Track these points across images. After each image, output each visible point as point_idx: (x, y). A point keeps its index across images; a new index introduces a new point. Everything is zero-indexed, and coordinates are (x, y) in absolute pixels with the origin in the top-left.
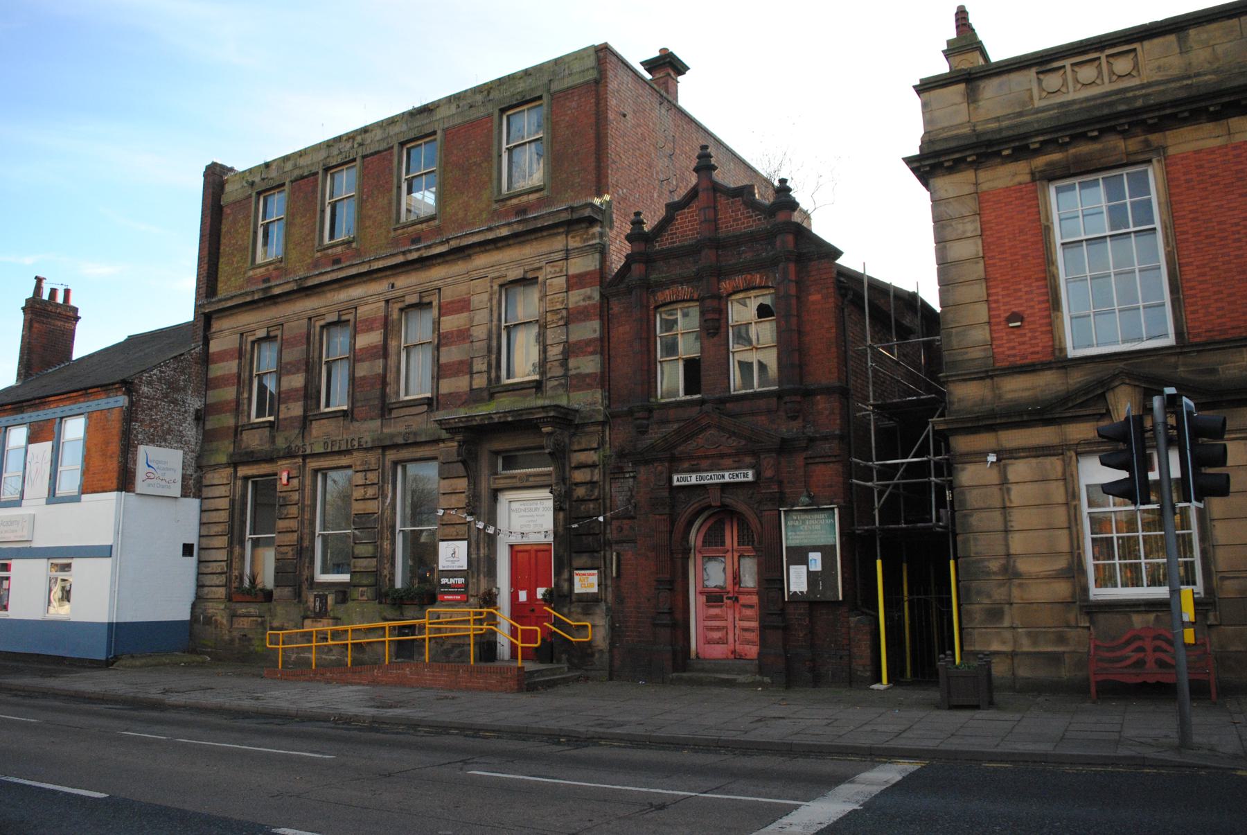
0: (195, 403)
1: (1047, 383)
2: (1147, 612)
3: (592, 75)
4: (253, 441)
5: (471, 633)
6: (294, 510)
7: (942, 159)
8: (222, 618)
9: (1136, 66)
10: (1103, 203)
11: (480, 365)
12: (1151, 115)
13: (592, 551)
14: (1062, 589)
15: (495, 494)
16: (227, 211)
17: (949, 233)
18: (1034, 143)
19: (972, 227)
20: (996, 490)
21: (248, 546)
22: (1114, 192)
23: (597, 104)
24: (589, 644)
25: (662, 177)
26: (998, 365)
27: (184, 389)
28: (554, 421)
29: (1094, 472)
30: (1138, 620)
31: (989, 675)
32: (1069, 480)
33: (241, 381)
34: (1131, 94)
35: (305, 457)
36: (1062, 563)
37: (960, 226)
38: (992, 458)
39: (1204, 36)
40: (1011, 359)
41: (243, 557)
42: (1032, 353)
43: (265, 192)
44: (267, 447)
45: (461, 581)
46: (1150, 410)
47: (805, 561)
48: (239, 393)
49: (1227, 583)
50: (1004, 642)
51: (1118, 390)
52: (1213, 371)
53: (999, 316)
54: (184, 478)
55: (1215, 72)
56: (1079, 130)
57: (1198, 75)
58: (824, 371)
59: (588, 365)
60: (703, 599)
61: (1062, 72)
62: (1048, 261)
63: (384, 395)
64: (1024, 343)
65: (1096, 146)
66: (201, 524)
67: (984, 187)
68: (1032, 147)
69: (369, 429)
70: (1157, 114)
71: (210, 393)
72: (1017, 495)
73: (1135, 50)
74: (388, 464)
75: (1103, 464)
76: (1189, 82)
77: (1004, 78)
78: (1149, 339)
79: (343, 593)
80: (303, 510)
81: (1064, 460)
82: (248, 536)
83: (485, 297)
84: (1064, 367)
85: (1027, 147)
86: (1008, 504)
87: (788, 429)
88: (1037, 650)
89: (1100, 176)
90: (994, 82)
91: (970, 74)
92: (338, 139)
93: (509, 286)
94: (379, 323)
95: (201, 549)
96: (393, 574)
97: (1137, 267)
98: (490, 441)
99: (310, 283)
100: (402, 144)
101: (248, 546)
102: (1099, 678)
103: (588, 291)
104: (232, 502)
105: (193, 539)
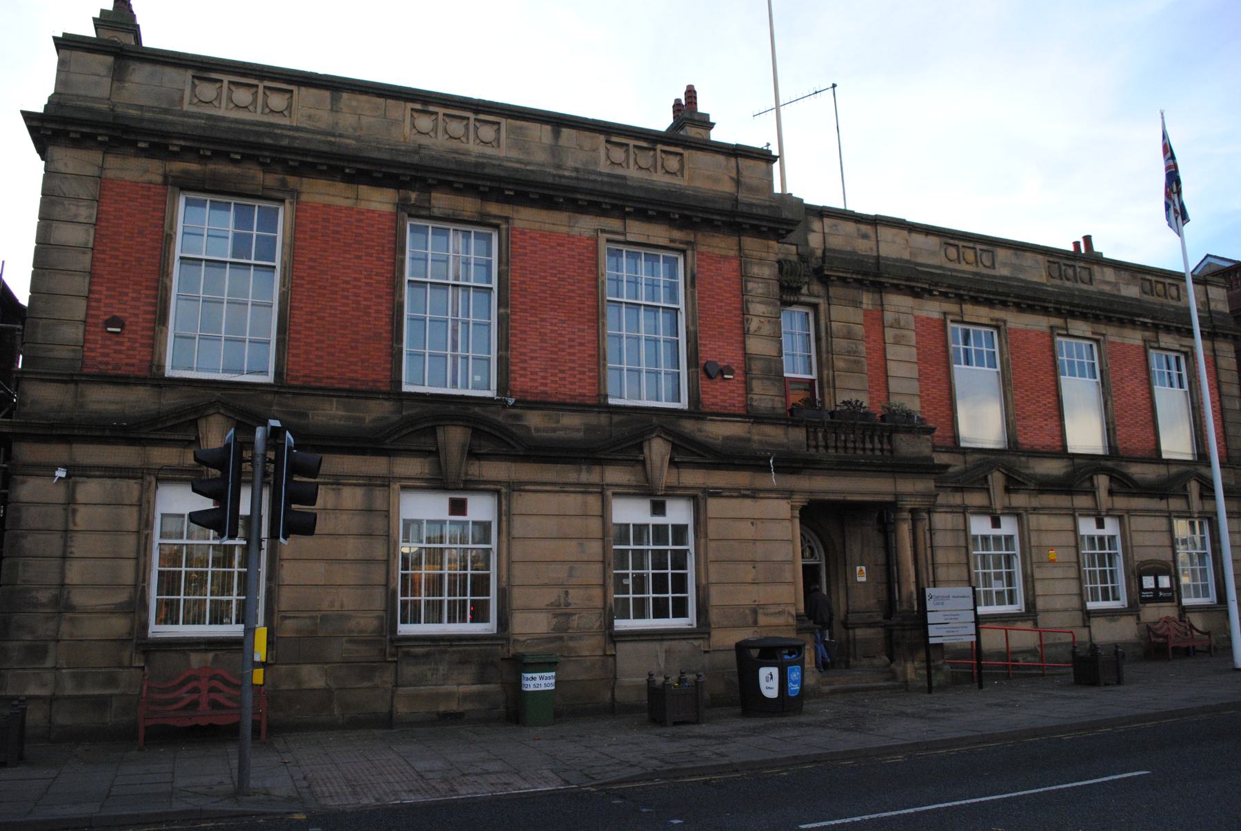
1: (138, 399)
2: (206, 651)
7: (70, 128)
9: (289, 107)
10: (231, 229)
12: (293, 157)
14: (119, 625)
17: (58, 212)
18: (175, 145)
19: (85, 213)
20: (59, 511)
22: (243, 220)
26: (86, 371)
29: (179, 501)
30: (196, 660)
31: (23, 722)
32: (144, 507)
34: (279, 131)
36: (123, 597)
37: (73, 208)
39: (354, 103)
40: (103, 367)
42: (127, 364)
46: (251, 444)
49: (287, 622)
50: (44, 685)
51: (211, 419)
52: (304, 415)
53: (97, 317)
55: (357, 139)
56: (224, 148)
57: (341, 136)
61: (218, 85)
62: (163, 271)
64: (120, 352)
65: (236, 170)
67: (110, 174)
68: (171, 148)
70: (299, 158)
72: (83, 517)
73: (291, 91)
75: (194, 490)
76: (333, 139)
77: (158, 68)
78: (249, 373)
81: (142, 485)
84: (159, 386)
85: (166, 146)
86: (71, 527)
88: (81, 693)
89: (233, 201)
90: (148, 68)
91: (121, 49)
97: (250, 300)
102: (150, 723)
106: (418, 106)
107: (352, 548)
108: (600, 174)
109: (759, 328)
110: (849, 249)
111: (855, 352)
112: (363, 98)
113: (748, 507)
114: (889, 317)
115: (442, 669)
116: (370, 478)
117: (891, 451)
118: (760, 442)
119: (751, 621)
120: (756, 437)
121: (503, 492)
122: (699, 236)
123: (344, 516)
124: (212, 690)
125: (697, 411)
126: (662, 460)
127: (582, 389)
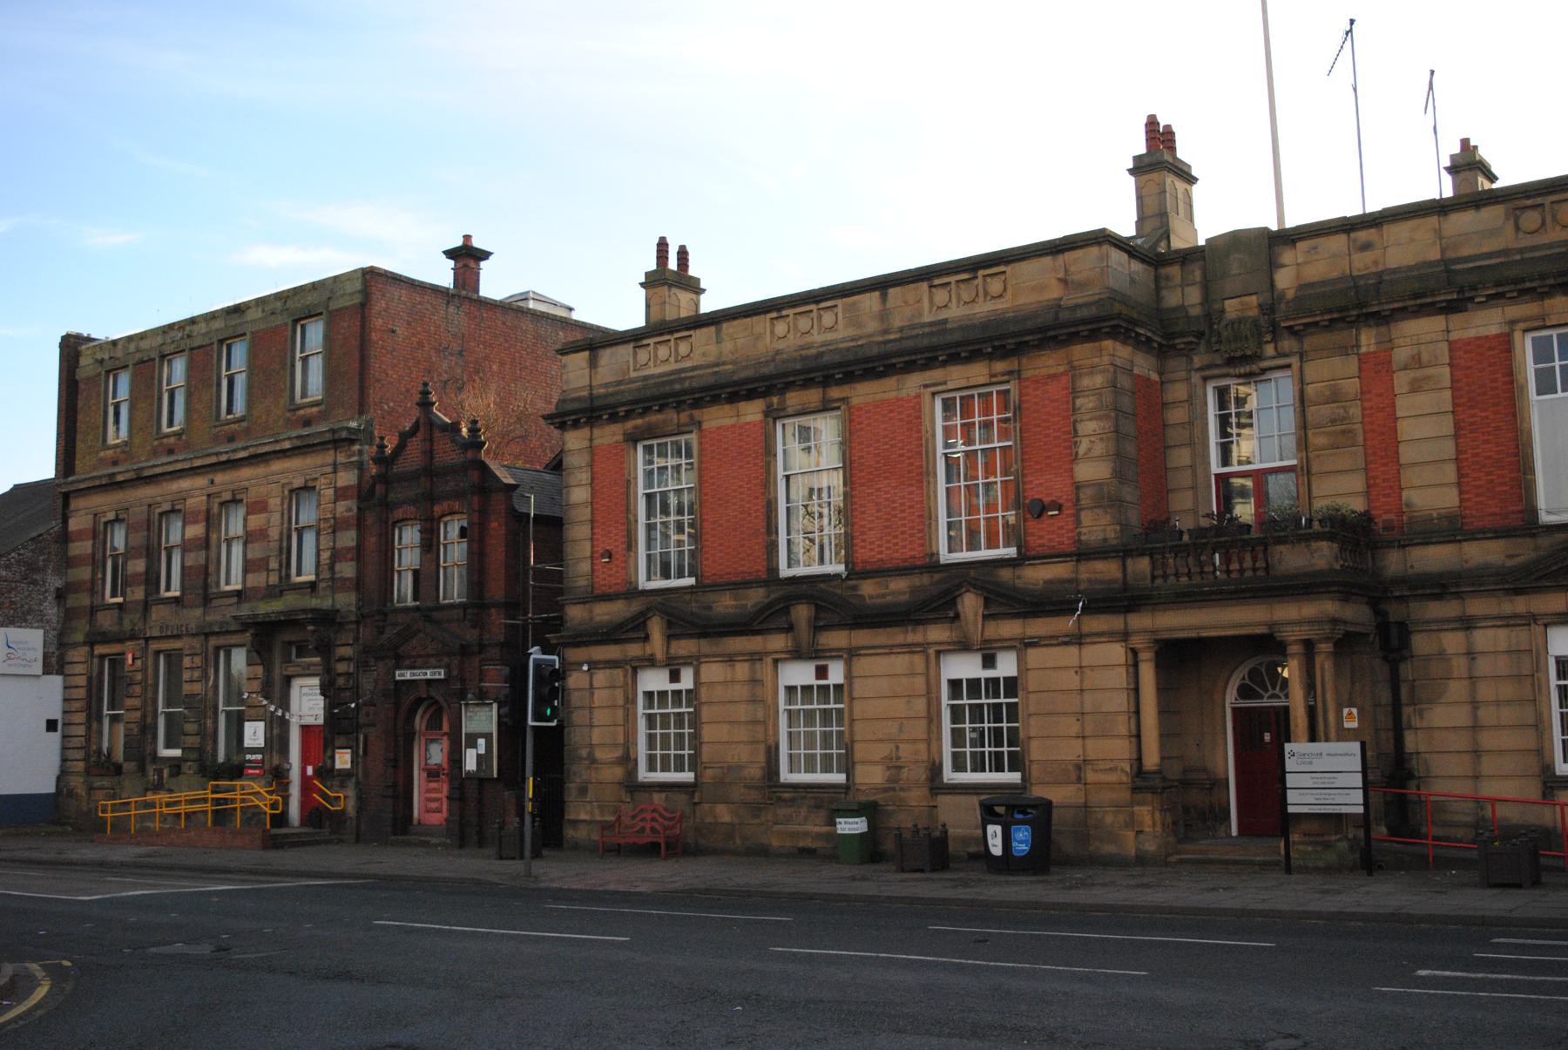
0: (55, 582)
3: (357, 299)
4: (106, 621)
5: (209, 807)
6: (138, 689)
8: (81, 791)
11: (274, 564)
13: (345, 733)
15: (287, 681)
16: (82, 386)
21: (106, 722)
23: (363, 327)
24: (343, 811)
25: (445, 377)
27: (43, 570)
28: (313, 621)
33: (96, 562)
35: (147, 640)
36: (619, 753)
38: (585, 668)
41: (100, 733)
43: (114, 371)
44: (115, 628)
45: (259, 757)
47: (475, 746)
48: (94, 573)
52: (709, 608)
54: (46, 656)
58: (497, 589)
59: (347, 570)
60: (424, 775)
63: (206, 586)
65: (660, 417)
66: (65, 700)
69: (194, 616)
71: (70, 571)
74: (211, 649)
77: (614, 349)
79: (175, 766)
80: (145, 689)
82: (105, 712)
83: (278, 501)
87: (471, 635)
92: (171, 326)
93: (296, 492)
94: (202, 517)
95: (64, 724)
96: (215, 750)
98: (278, 637)
99: (146, 473)
100: (221, 342)
101: (106, 722)
103: (349, 503)
104: (90, 679)
105: (57, 714)
106: (774, 315)
107: (743, 712)
108: (923, 325)
109: (1089, 450)
110: (1335, 274)
111: (1344, 418)
112: (736, 323)
113: (1070, 655)
114: (1401, 355)
115: (804, 811)
116: (751, 654)
117: (1267, 568)
118: (1089, 580)
119: (1074, 777)
120: (1084, 576)
121: (850, 655)
122: (1024, 360)
123: (738, 687)
124: (653, 819)
125: (856, 572)
126: (976, 615)
127: (906, 551)
